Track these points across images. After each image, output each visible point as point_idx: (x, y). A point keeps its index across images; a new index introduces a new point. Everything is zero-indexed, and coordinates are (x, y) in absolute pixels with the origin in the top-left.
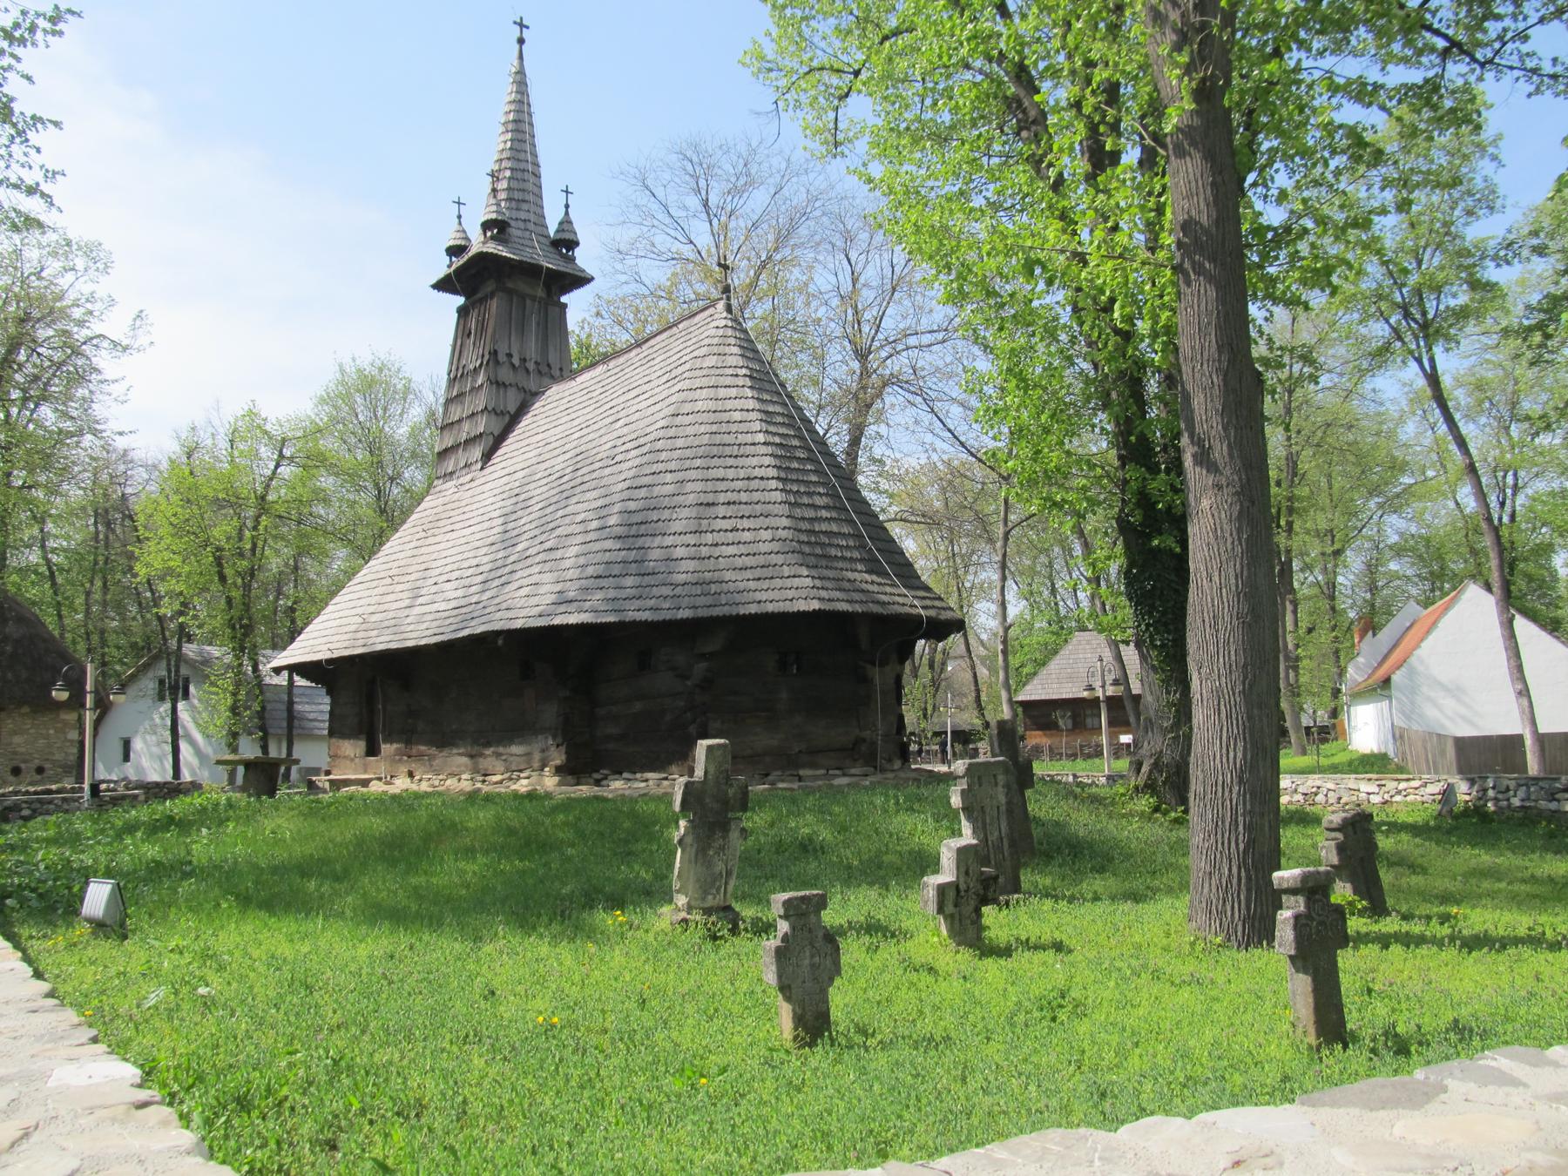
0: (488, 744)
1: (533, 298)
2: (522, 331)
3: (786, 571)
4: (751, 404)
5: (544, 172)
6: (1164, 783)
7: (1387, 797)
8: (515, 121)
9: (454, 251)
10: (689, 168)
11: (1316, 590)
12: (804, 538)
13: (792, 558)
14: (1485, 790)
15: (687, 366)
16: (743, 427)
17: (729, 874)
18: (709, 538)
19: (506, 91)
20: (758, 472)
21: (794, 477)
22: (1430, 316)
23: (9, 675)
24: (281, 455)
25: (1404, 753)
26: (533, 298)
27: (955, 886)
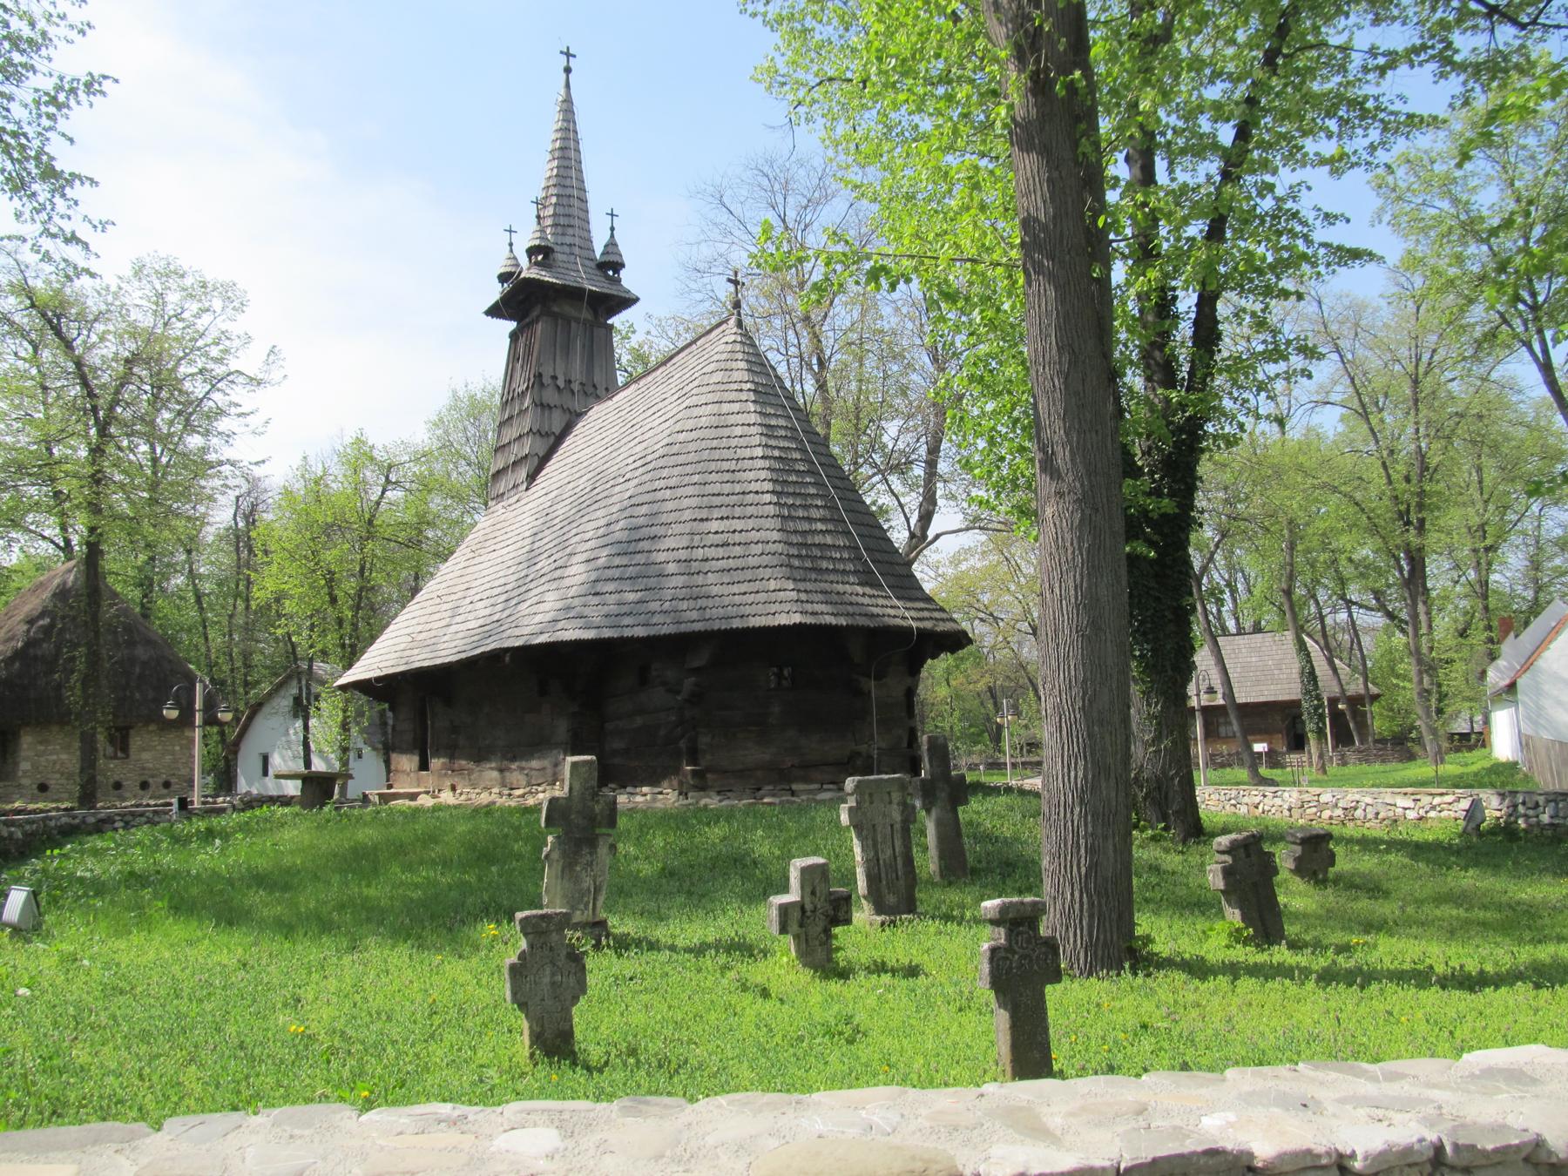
0: (514, 759)
1: (577, 320)
2: (567, 351)
3: (772, 585)
4: (753, 418)
5: (591, 197)
6: (1145, 799)
7: (1422, 812)
8: (561, 148)
9: (503, 278)
10: (765, 182)
11: (1468, 589)
12: (794, 551)
13: (779, 572)
14: (1515, 806)
15: (696, 383)
16: (743, 442)
17: (597, 890)
18: (699, 553)
19: (553, 119)
20: (754, 487)
21: (791, 490)
22: (1540, 299)
23: (137, 696)
24: (388, 481)
25: (1530, 762)
26: (577, 320)
27: (801, 906)
